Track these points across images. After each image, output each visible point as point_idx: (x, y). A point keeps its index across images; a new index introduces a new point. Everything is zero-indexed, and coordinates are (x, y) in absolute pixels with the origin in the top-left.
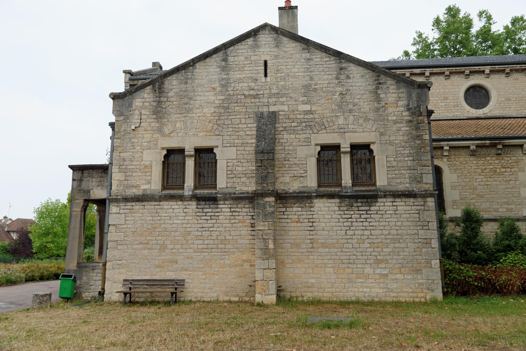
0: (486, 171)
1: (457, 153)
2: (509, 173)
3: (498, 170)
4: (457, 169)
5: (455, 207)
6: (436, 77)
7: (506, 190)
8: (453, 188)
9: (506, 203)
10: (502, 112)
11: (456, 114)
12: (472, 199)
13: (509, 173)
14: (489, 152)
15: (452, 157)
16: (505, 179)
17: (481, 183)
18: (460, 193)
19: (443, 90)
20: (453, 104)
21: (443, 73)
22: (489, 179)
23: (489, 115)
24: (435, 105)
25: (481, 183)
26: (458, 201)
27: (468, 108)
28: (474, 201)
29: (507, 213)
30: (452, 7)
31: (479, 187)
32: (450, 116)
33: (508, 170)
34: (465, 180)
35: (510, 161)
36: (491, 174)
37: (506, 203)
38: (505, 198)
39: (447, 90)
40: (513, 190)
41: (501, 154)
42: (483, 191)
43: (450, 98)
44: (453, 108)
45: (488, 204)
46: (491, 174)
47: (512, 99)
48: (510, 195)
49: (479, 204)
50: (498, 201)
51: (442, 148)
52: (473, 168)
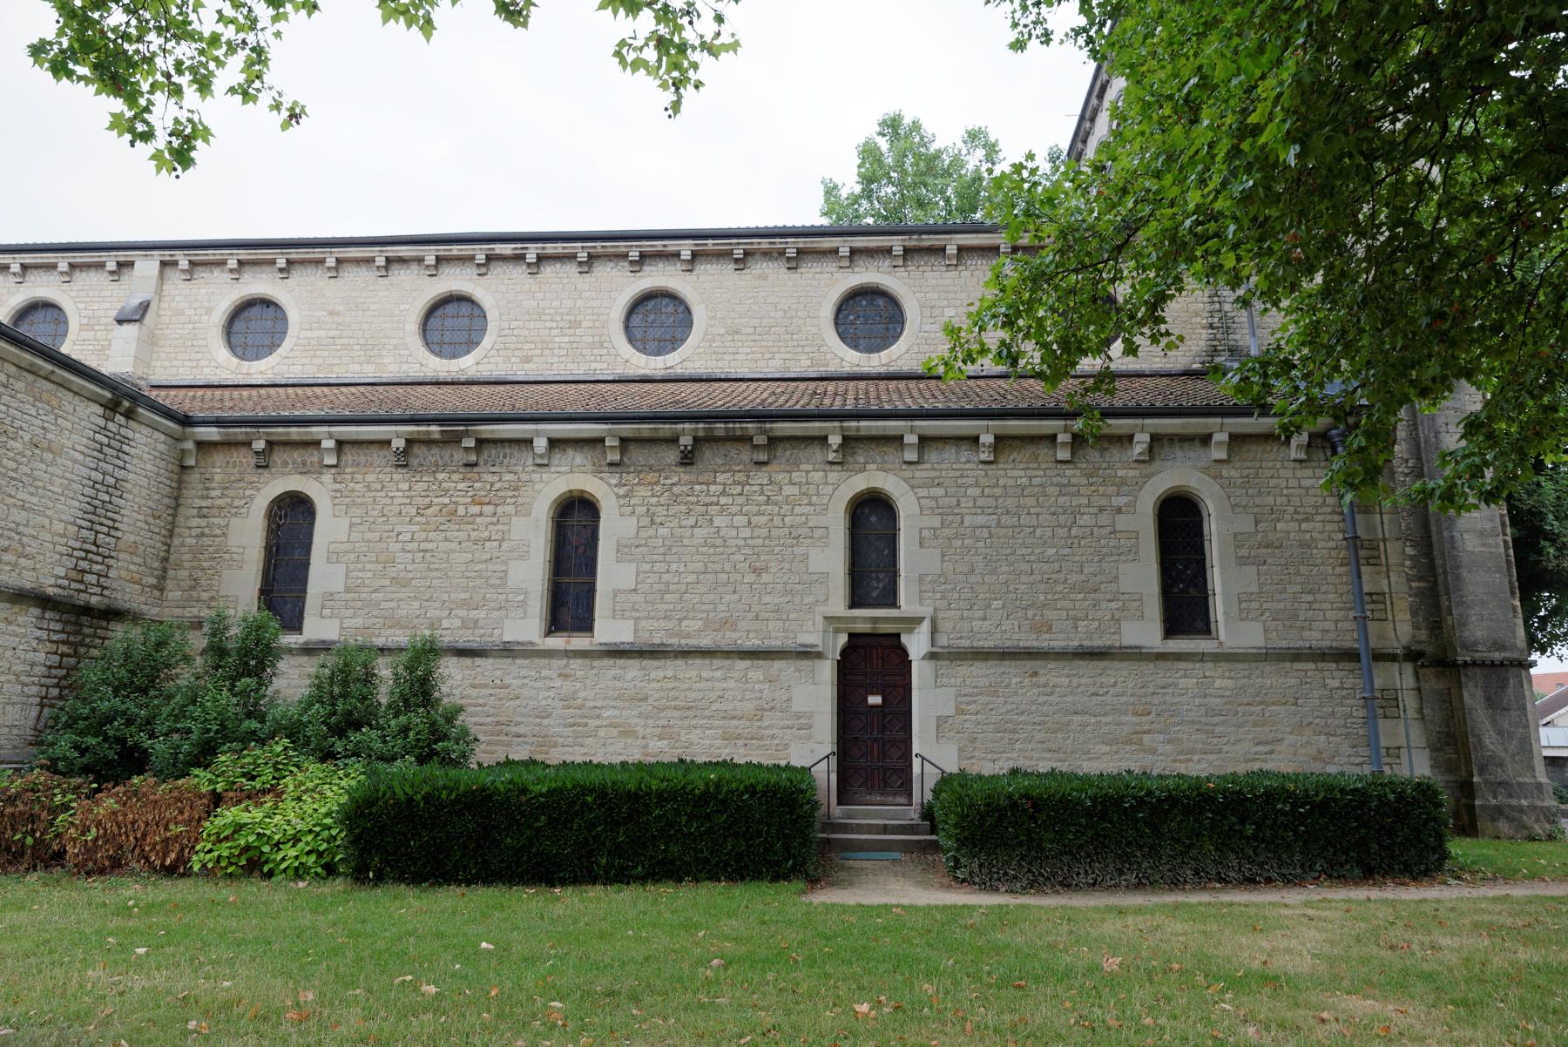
0: (429, 511)
1: (362, 459)
2: (489, 520)
3: (461, 510)
4: (354, 504)
5: (326, 612)
6: (558, 266)
7: (471, 567)
8: (333, 557)
9: (464, 604)
10: (714, 364)
11: (594, 366)
12: (376, 591)
13: (489, 520)
14: (447, 458)
15: (348, 470)
16: (474, 535)
17: (409, 546)
18: (348, 572)
19: (569, 303)
20: (590, 339)
21: (573, 257)
22: (432, 535)
23: (679, 371)
24: (543, 342)
25: (409, 546)
26: (337, 596)
27: (627, 350)
28: (380, 596)
29: (461, 632)
30: (907, 121)
31: (401, 557)
32: (579, 371)
33: (488, 509)
34: (369, 535)
35: (497, 486)
36: (441, 519)
37: (464, 604)
38: (466, 589)
39: (580, 303)
40: (491, 567)
41: (476, 465)
42: (409, 567)
43: (585, 324)
44: (588, 352)
45: (416, 604)
46: (441, 519)
47: (744, 330)
48: (478, 582)
49: (394, 604)
50: (445, 597)
51: (318, 443)
52: (397, 501)
